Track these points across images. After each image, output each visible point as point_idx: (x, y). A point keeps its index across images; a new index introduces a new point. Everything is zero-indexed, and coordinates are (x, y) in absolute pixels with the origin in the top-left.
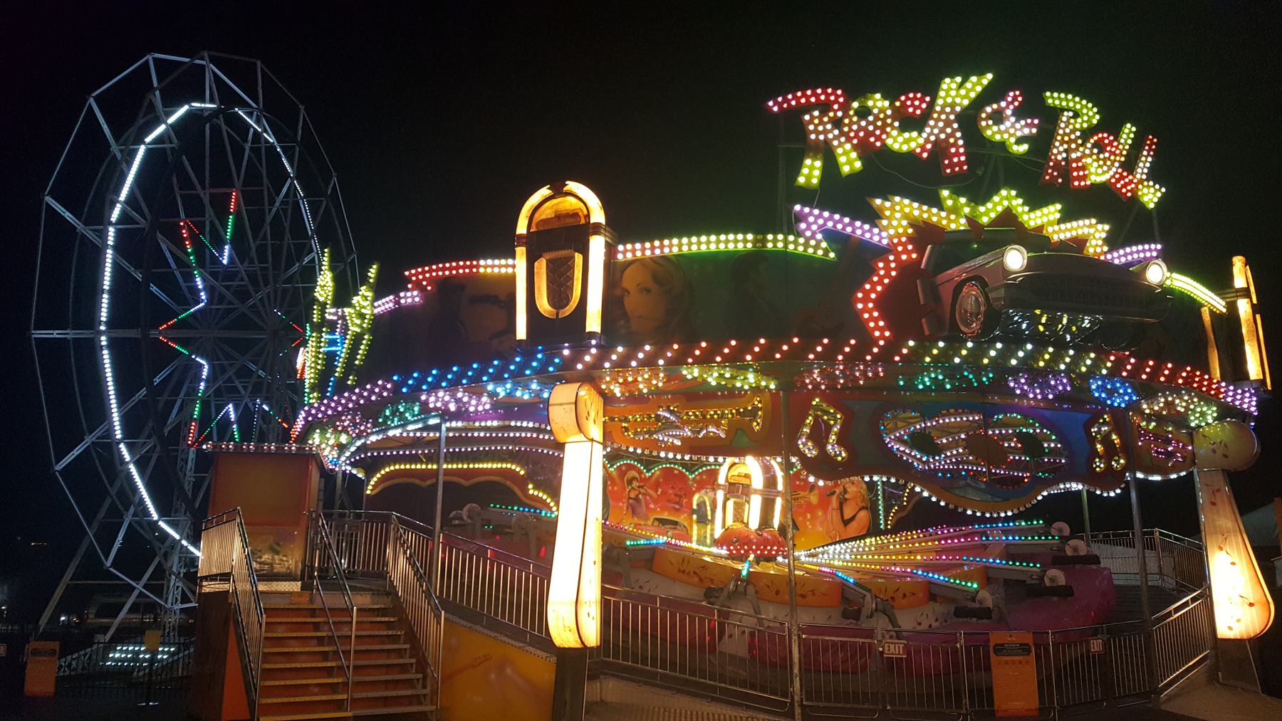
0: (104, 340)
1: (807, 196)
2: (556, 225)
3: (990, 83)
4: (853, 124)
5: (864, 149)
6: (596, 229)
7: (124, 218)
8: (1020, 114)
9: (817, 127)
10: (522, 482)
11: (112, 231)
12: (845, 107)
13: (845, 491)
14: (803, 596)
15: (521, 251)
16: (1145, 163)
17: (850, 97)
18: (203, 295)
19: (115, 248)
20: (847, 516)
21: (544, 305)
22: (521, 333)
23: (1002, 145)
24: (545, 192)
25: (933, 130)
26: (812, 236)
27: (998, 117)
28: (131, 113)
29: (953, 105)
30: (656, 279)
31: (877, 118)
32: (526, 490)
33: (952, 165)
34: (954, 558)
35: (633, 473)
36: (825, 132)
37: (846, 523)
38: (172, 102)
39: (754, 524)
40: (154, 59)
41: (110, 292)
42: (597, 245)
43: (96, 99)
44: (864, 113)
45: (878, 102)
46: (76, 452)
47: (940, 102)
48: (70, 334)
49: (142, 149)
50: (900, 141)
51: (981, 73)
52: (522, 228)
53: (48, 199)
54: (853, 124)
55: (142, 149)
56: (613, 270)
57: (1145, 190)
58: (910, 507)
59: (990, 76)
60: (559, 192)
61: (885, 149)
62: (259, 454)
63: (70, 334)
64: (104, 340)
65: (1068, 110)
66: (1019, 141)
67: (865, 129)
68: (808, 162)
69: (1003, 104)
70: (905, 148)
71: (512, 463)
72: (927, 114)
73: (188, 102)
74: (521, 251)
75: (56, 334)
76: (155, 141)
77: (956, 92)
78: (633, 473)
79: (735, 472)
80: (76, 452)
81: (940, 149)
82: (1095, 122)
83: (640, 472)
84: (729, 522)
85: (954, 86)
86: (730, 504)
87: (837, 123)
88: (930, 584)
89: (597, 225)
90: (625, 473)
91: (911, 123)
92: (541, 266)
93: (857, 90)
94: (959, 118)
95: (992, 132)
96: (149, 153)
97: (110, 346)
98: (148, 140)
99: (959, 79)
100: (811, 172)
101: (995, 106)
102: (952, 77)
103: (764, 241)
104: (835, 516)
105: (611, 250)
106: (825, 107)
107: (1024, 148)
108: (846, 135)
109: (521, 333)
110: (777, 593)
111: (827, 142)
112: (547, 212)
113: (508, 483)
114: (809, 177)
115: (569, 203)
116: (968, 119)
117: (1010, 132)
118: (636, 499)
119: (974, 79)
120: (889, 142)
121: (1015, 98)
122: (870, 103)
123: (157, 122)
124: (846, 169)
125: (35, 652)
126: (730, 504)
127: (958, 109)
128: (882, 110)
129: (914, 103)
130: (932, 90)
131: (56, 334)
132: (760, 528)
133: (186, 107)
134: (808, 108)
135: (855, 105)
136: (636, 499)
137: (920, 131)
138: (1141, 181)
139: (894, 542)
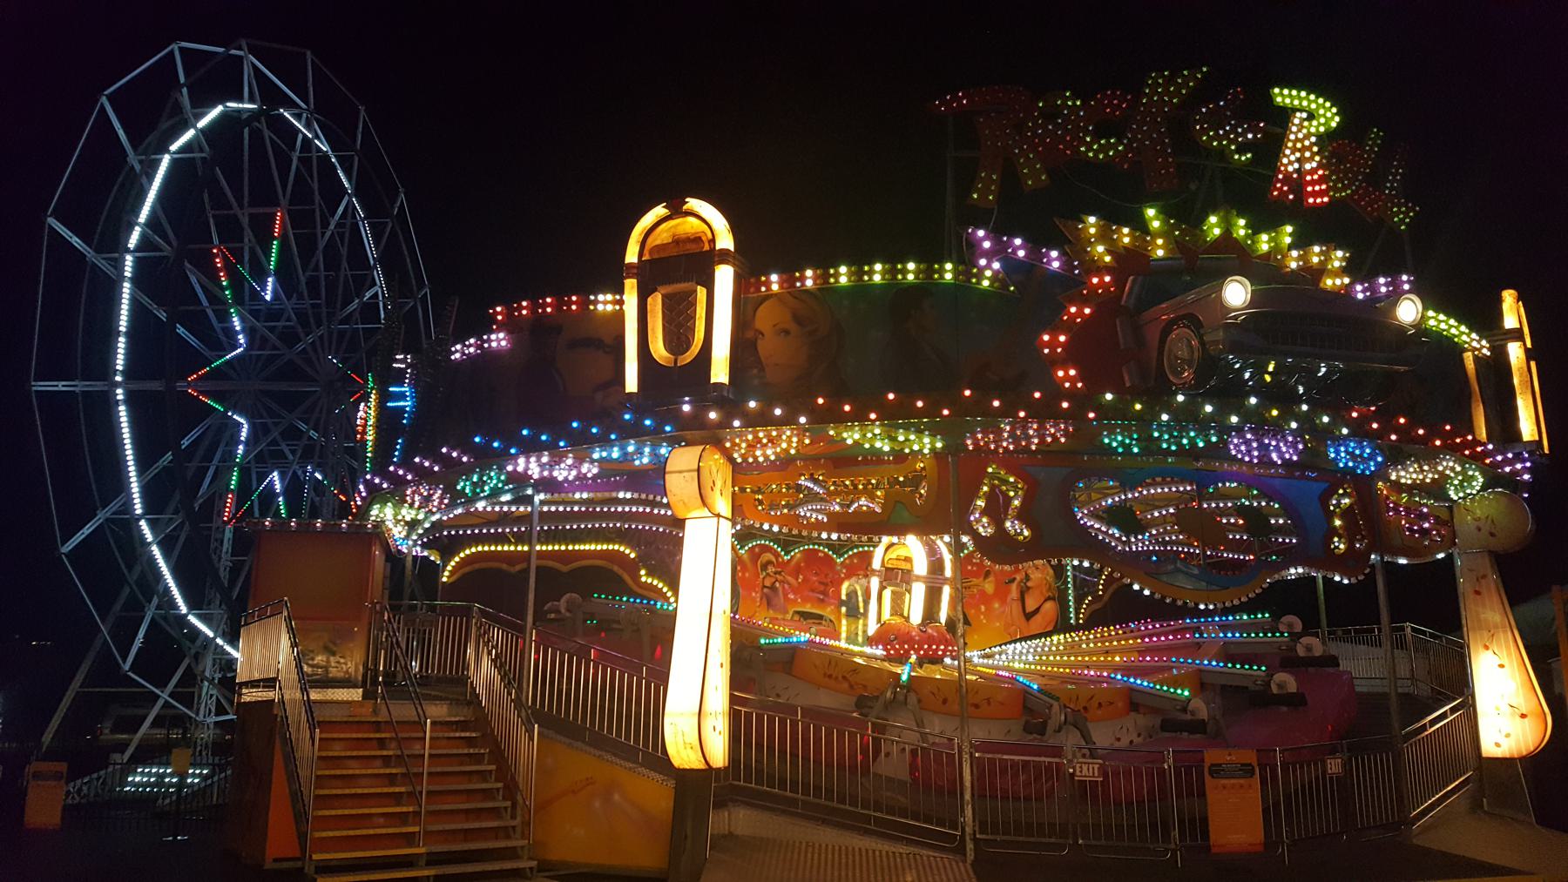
0: (120, 394)
2: (674, 252)
10: (632, 568)
11: (129, 260)
13: (1028, 578)
14: (976, 706)
15: (631, 285)
18: (241, 339)
19: (135, 281)
20: (1031, 607)
21: (659, 350)
24: (660, 211)
30: (798, 319)
32: (637, 577)
34: (1160, 659)
35: (768, 556)
37: (1029, 616)
39: (916, 617)
40: (181, 49)
43: (109, 98)
44: (1051, 114)
46: (87, 530)
48: (79, 386)
49: (166, 160)
52: (632, 256)
53: (51, 221)
55: (166, 160)
58: (1106, 598)
60: (677, 211)
63: (79, 386)
64: (120, 394)
65: (1301, 111)
71: (621, 543)
73: (222, 102)
74: (631, 285)
75: (61, 386)
76: (182, 150)
78: (768, 556)
79: (893, 554)
82: (1334, 124)
83: (777, 555)
84: (886, 615)
86: (887, 594)
88: (1132, 690)
90: (759, 555)
92: (656, 302)
96: (175, 163)
98: (174, 148)
104: (1016, 607)
110: (945, 701)
112: (663, 235)
113: (616, 568)
115: (690, 225)
118: (772, 588)
126: (887, 594)
131: (61, 386)
132: (923, 623)
133: (220, 108)
136: (772, 588)
139: (1088, 640)
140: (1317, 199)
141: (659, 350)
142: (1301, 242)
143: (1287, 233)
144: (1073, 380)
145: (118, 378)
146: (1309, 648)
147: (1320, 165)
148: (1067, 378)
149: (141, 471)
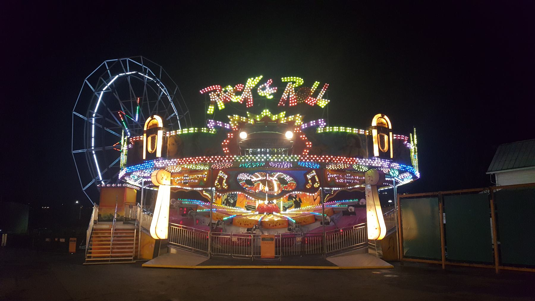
0: (94, 152)
1: (211, 117)
2: (152, 127)
3: (262, 79)
4: (223, 95)
5: (225, 102)
6: (159, 129)
7: (96, 116)
8: (271, 86)
9: (213, 97)
11: (93, 119)
12: (220, 91)
15: (145, 135)
16: (323, 92)
17: (222, 87)
18: (129, 134)
19: (92, 124)
21: (150, 150)
22: (144, 158)
23: (265, 97)
24: (150, 119)
25: (244, 95)
26: (211, 127)
27: (264, 89)
28: (98, 84)
29: (250, 87)
30: (176, 141)
31: (229, 93)
32: (203, 193)
33: (249, 104)
36: (215, 98)
38: (113, 75)
40: (107, 62)
41: (95, 137)
42: (160, 133)
43: (87, 80)
44: (225, 92)
45: (230, 88)
46: (90, 184)
47: (246, 86)
48: (85, 150)
49: (102, 93)
50: (235, 99)
51: (259, 76)
52: (145, 129)
53: (74, 113)
54: (223, 95)
55: (102, 93)
56: (165, 139)
57: (320, 102)
59: (261, 77)
60: (153, 119)
61: (231, 101)
62: (117, 187)
63: (85, 150)
64: (94, 152)
65: (290, 82)
66: (270, 95)
67: (225, 97)
68: (210, 107)
69: (266, 84)
70: (236, 101)
72: (243, 90)
73: (118, 74)
74: (145, 135)
75: (80, 151)
76: (106, 90)
77: (251, 83)
80: (90, 184)
81: (246, 100)
82: (301, 84)
85: (251, 81)
87: (218, 95)
89: (160, 128)
91: (238, 93)
92: (150, 139)
93: (224, 85)
94: (251, 90)
95: (261, 93)
96: (104, 93)
97: (96, 153)
98: (104, 89)
99: (252, 79)
100: (211, 110)
101: (263, 85)
102: (250, 78)
103: (198, 130)
105: (165, 134)
106: (215, 91)
107: (272, 97)
108: (220, 99)
109: (144, 158)
111: (215, 101)
112: (150, 124)
114: (221, 106)
115: (154, 121)
116: (254, 91)
117: (268, 92)
119: (257, 78)
120: (232, 99)
121: (270, 82)
122: (227, 89)
123: (105, 85)
124: (220, 108)
125: (71, 241)
127: (251, 88)
128: (230, 91)
129: (239, 87)
130: (244, 82)
131: (80, 151)
133: (117, 76)
134: (210, 92)
135: (223, 89)
137: (241, 95)
138: (319, 100)
140: (293, 103)
141: (150, 150)
142: (287, 116)
143: (282, 114)
144: (304, 138)
145: (93, 148)
146: (351, 210)
147: (294, 95)
148: (303, 137)
149: (101, 171)
